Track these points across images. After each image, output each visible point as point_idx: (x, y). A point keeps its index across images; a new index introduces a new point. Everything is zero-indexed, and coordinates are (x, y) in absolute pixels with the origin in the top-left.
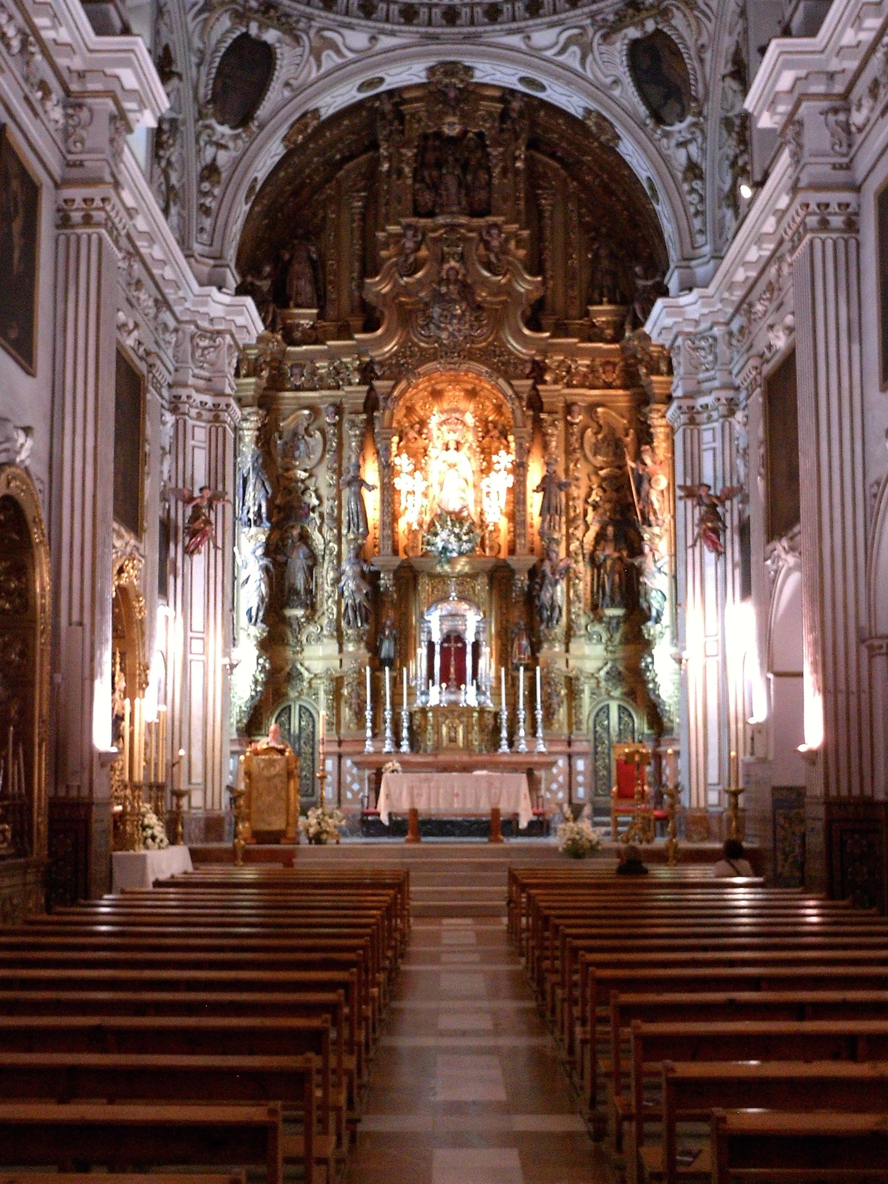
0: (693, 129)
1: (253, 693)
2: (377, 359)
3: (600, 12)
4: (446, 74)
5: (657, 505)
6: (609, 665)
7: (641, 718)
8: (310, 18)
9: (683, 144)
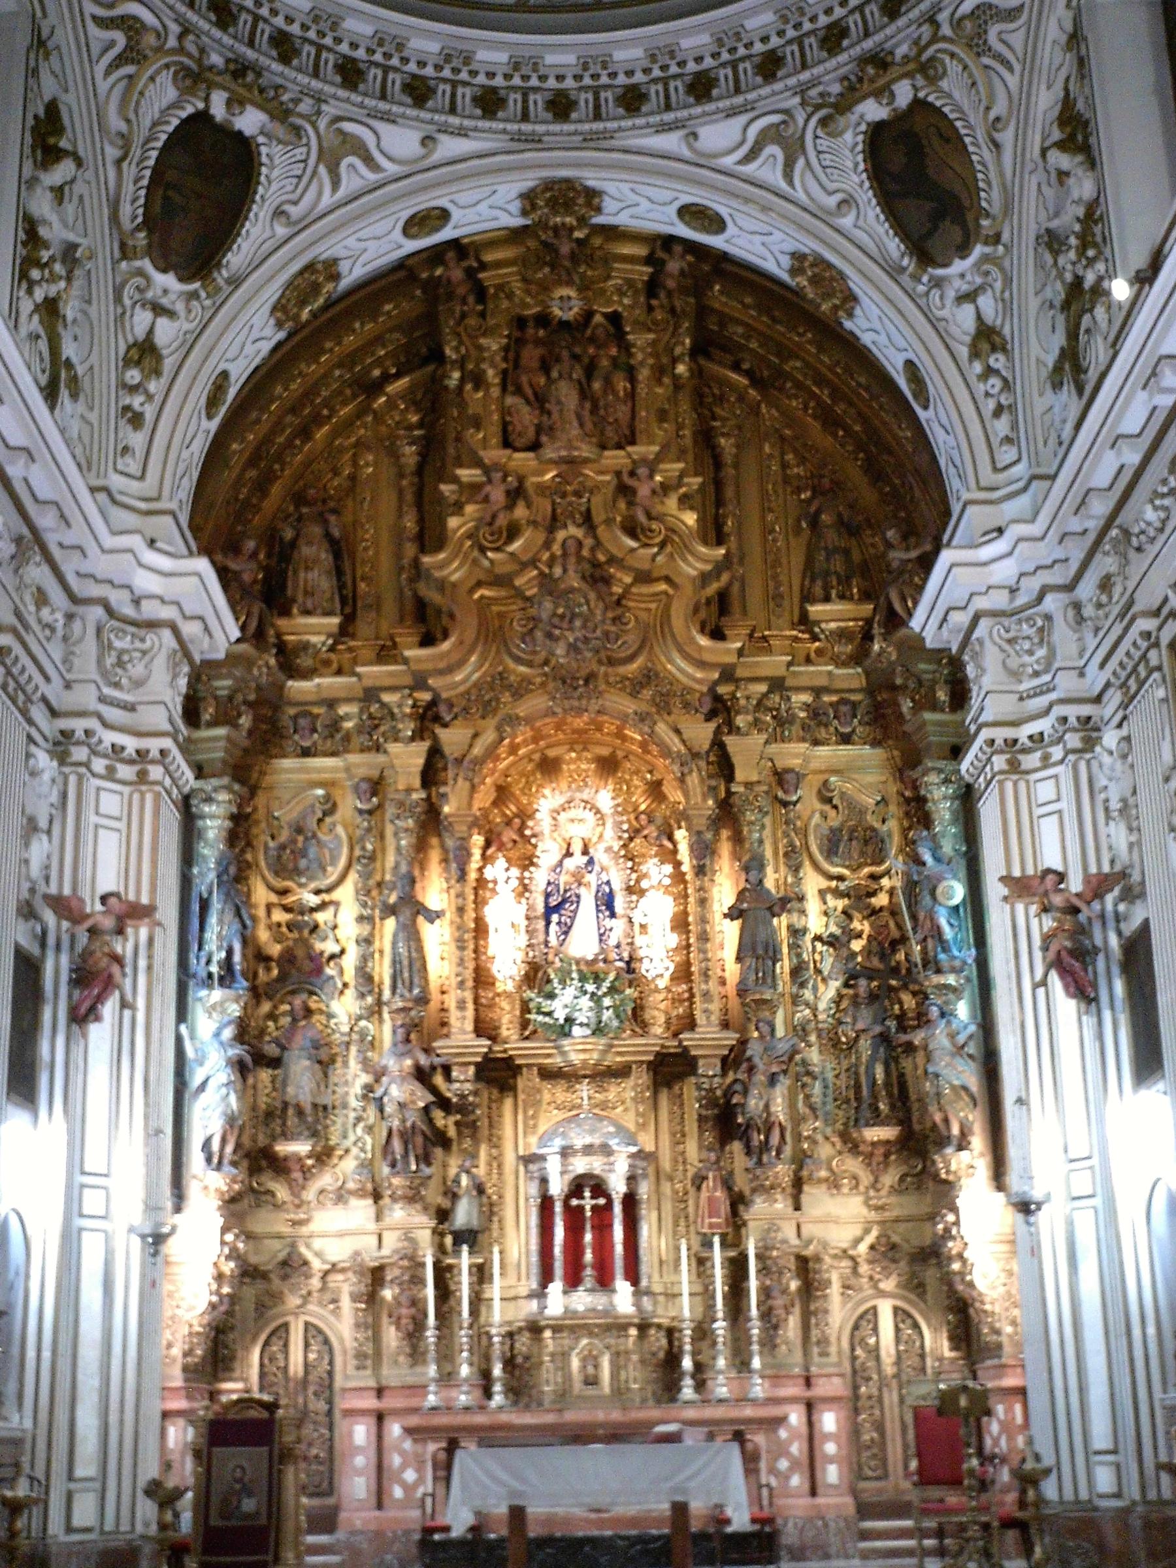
0: (986, 267)
1: (215, 1299)
2: (444, 695)
3: (814, 82)
4: (554, 205)
5: (948, 933)
6: (875, 1233)
7: (935, 1330)
8: (319, 99)
9: (969, 297)
